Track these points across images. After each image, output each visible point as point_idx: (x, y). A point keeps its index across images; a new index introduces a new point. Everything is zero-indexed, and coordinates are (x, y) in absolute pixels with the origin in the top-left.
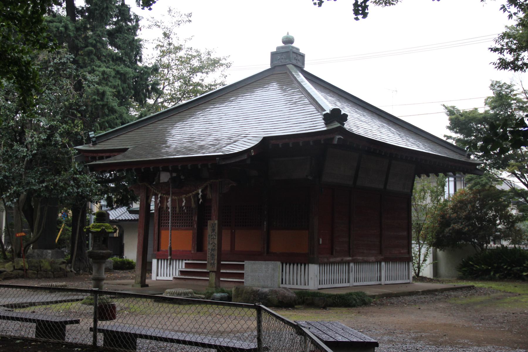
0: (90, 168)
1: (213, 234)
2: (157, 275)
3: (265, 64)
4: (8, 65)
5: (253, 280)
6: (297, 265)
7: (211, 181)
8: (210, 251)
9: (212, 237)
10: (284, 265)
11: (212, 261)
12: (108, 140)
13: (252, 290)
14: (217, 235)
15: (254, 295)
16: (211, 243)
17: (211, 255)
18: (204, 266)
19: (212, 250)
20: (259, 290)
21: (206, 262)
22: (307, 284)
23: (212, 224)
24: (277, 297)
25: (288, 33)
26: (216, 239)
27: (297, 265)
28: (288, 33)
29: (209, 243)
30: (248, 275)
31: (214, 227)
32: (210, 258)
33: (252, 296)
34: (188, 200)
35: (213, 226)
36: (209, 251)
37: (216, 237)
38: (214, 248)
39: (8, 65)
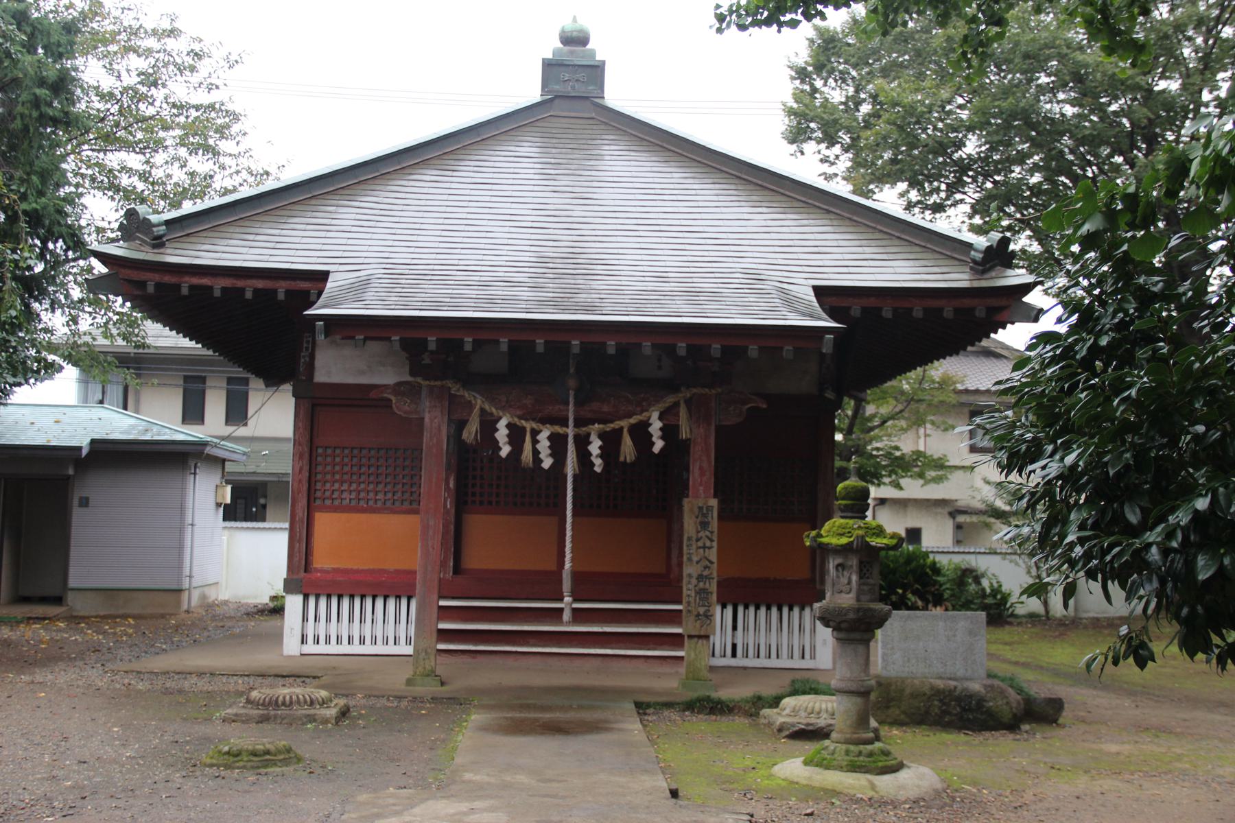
0: (326, 325)
1: (700, 535)
2: (303, 640)
3: (529, 91)
4: (919, 9)
5: (909, 660)
6: (780, 609)
7: (695, 390)
8: (694, 581)
9: (700, 544)
10: (741, 609)
11: (702, 610)
12: (188, 235)
13: (932, 688)
14: (715, 538)
15: (941, 701)
16: (695, 559)
17: (697, 593)
18: (674, 617)
19: (700, 578)
20: (955, 687)
21: (442, 603)
22: (807, 655)
23: (700, 508)
24: (1007, 703)
25: (575, 18)
26: (714, 550)
27: (780, 609)
28: (575, 18)
29: (690, 559)
30: (892, 648)
31: (705, 515)
32: (692, 600)
33: (936, 703)
34: (611, 443)
35: (703, 512)
36: (689, 583)
37: (715, 544)
38: (706, 573)
39: (919, 9)
